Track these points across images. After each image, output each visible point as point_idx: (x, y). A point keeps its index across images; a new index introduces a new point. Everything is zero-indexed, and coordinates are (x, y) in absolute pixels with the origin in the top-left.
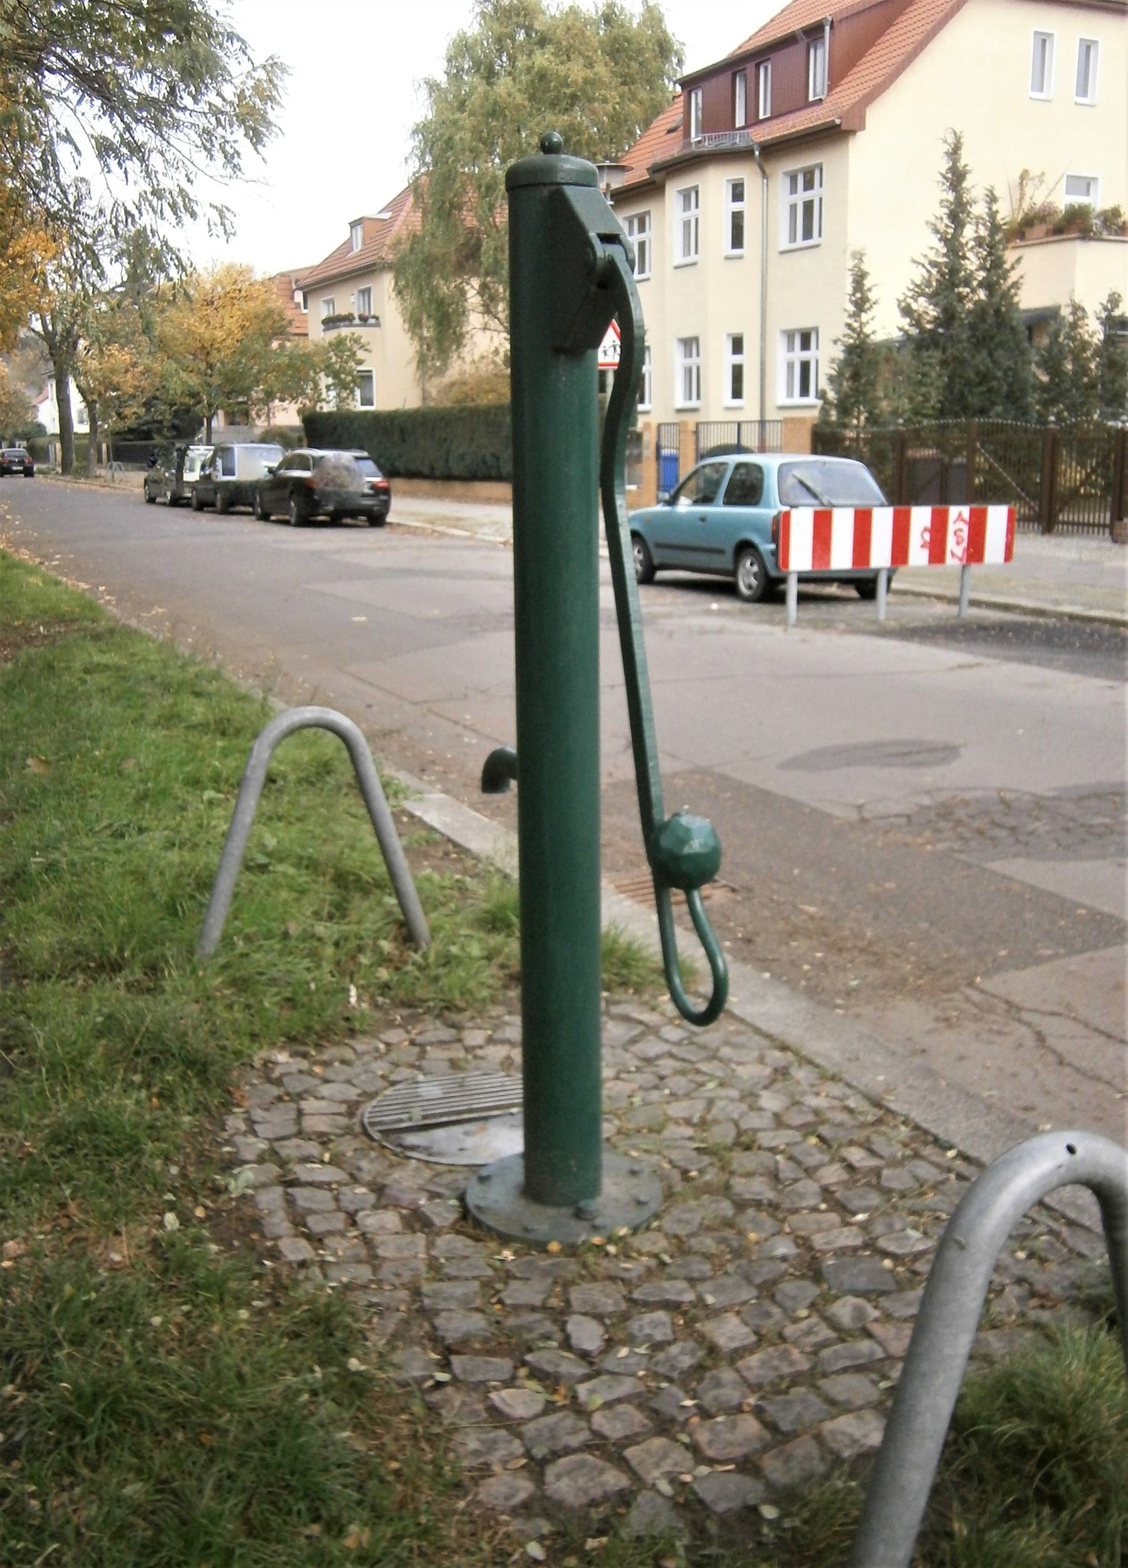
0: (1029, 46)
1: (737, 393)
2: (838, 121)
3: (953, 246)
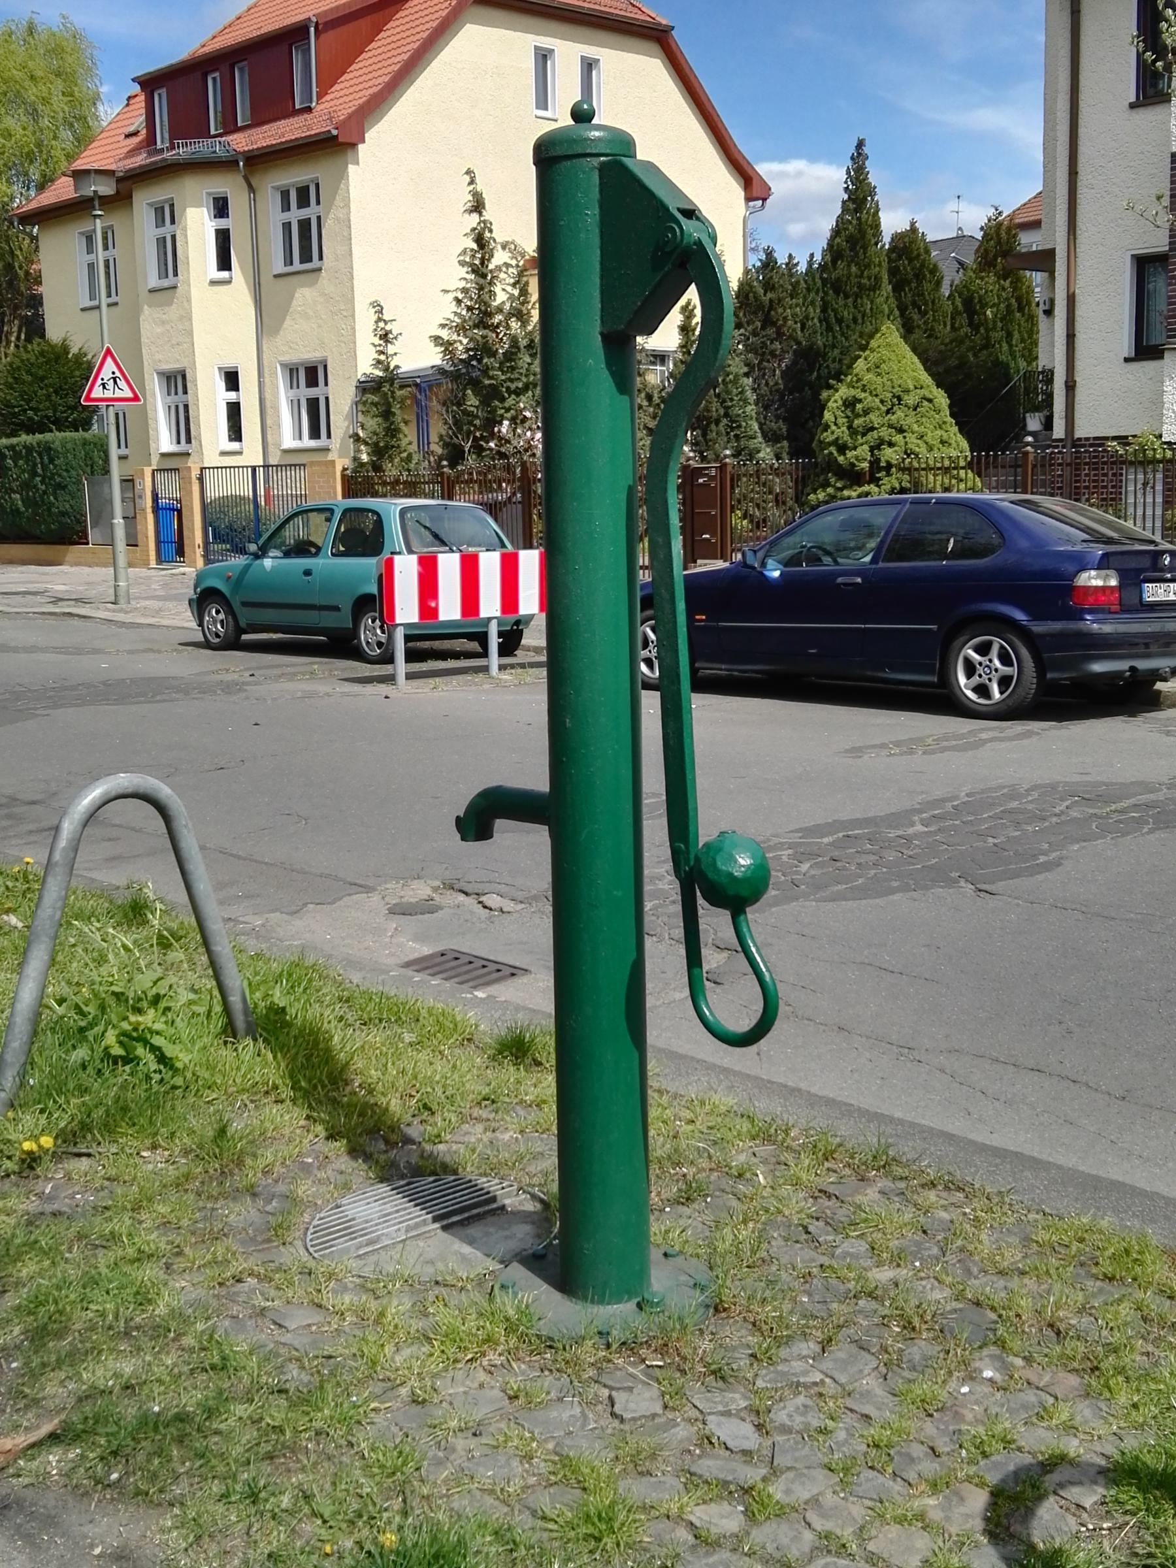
0: (529, 63)
1: (236, 433)
2: (335, 132)
3: (480, 271)
